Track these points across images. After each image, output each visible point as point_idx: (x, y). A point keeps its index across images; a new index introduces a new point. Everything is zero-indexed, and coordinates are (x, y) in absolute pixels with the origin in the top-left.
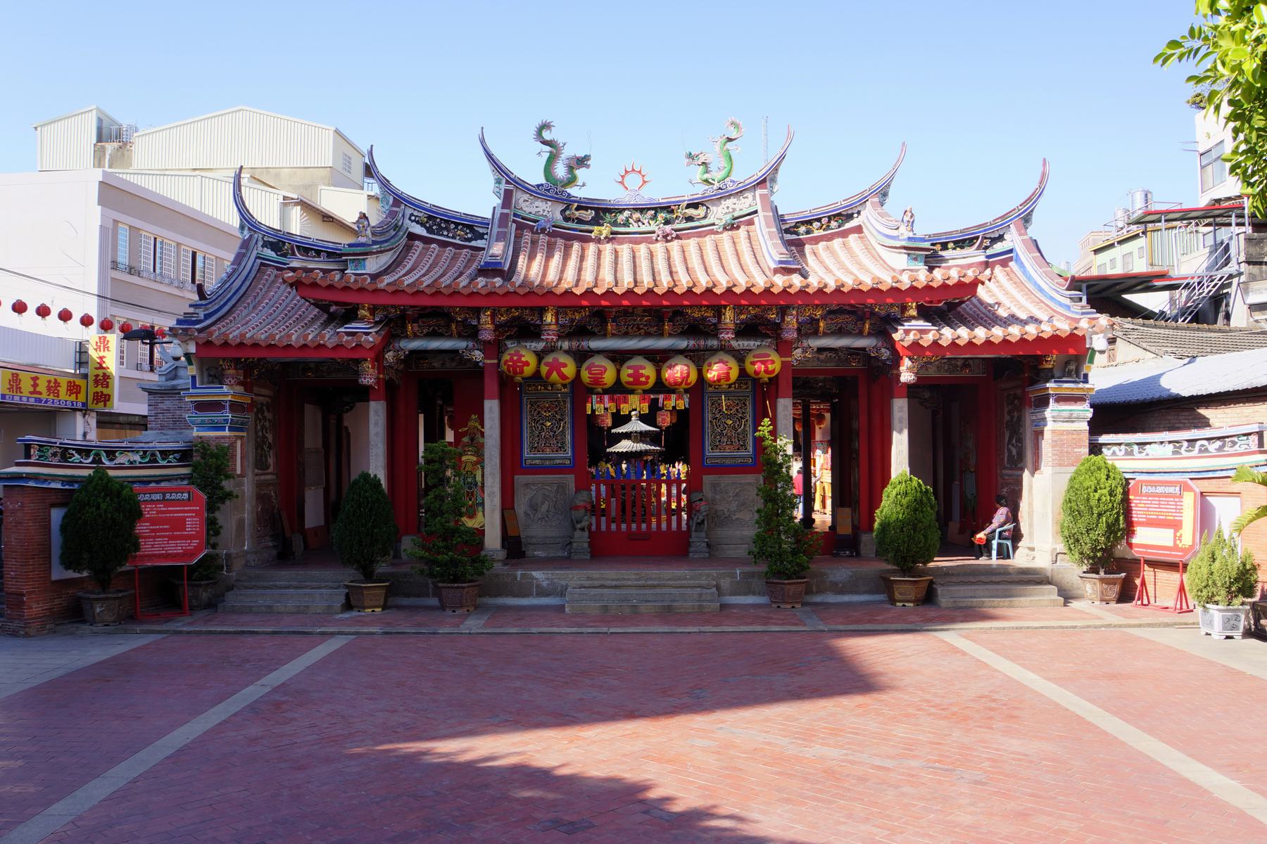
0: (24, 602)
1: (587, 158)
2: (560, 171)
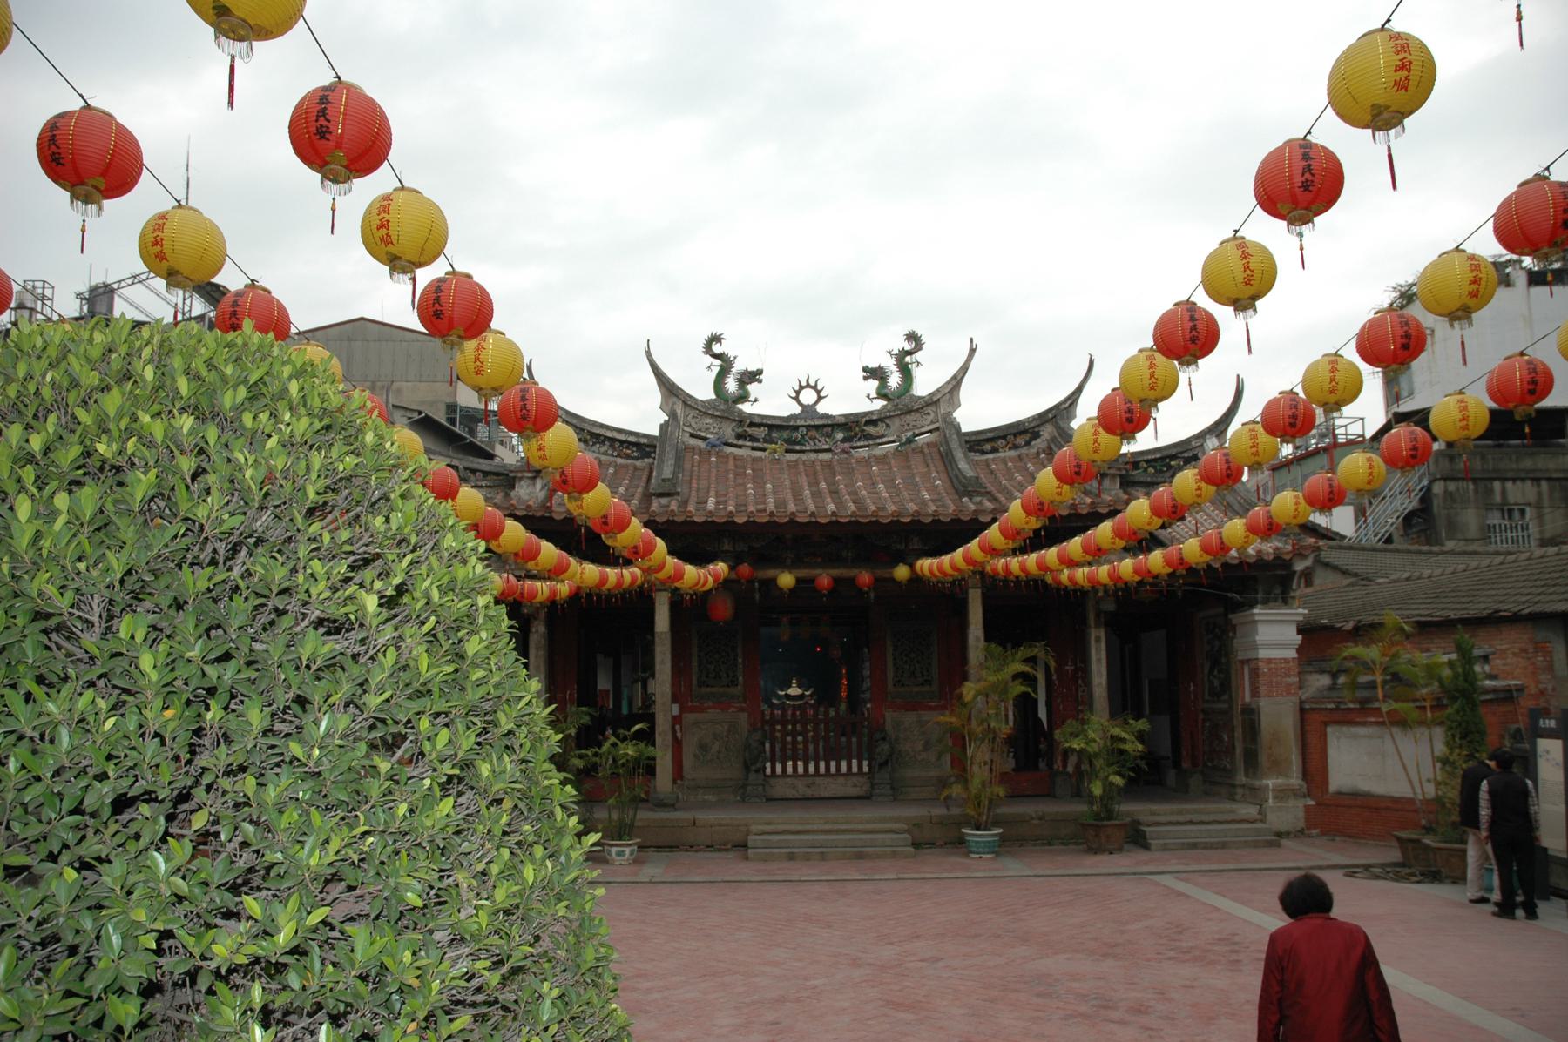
1: (760, 372)
2: (731, 385)
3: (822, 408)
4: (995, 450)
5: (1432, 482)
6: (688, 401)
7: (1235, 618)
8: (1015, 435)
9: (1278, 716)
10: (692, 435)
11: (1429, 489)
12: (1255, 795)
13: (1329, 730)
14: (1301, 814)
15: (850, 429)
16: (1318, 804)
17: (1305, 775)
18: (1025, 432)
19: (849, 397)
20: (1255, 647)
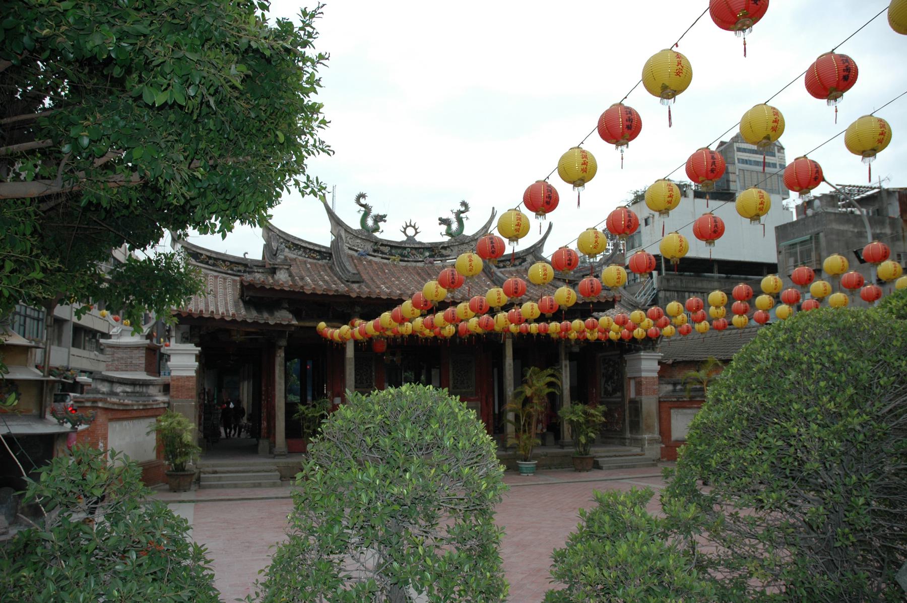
0: (294, 478)
1: (385, 216)
2: (370, 222)
3: (418, 238)
4: (504, 267)
5: (658, 291)
6: (347, 229)
7: (626, 357)
8: (515, 259)
9: (649, 404)
10: (349, 248)
11: (657, 295)
12: (638, 442)
13: (672, 411)
14: (659, 451)
15: (433, 251)
16: (667, 446)
17: (661, 433)
18: (519, 258)
19: (432, 234)
20: (640, 371)
